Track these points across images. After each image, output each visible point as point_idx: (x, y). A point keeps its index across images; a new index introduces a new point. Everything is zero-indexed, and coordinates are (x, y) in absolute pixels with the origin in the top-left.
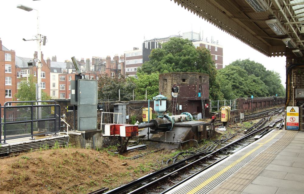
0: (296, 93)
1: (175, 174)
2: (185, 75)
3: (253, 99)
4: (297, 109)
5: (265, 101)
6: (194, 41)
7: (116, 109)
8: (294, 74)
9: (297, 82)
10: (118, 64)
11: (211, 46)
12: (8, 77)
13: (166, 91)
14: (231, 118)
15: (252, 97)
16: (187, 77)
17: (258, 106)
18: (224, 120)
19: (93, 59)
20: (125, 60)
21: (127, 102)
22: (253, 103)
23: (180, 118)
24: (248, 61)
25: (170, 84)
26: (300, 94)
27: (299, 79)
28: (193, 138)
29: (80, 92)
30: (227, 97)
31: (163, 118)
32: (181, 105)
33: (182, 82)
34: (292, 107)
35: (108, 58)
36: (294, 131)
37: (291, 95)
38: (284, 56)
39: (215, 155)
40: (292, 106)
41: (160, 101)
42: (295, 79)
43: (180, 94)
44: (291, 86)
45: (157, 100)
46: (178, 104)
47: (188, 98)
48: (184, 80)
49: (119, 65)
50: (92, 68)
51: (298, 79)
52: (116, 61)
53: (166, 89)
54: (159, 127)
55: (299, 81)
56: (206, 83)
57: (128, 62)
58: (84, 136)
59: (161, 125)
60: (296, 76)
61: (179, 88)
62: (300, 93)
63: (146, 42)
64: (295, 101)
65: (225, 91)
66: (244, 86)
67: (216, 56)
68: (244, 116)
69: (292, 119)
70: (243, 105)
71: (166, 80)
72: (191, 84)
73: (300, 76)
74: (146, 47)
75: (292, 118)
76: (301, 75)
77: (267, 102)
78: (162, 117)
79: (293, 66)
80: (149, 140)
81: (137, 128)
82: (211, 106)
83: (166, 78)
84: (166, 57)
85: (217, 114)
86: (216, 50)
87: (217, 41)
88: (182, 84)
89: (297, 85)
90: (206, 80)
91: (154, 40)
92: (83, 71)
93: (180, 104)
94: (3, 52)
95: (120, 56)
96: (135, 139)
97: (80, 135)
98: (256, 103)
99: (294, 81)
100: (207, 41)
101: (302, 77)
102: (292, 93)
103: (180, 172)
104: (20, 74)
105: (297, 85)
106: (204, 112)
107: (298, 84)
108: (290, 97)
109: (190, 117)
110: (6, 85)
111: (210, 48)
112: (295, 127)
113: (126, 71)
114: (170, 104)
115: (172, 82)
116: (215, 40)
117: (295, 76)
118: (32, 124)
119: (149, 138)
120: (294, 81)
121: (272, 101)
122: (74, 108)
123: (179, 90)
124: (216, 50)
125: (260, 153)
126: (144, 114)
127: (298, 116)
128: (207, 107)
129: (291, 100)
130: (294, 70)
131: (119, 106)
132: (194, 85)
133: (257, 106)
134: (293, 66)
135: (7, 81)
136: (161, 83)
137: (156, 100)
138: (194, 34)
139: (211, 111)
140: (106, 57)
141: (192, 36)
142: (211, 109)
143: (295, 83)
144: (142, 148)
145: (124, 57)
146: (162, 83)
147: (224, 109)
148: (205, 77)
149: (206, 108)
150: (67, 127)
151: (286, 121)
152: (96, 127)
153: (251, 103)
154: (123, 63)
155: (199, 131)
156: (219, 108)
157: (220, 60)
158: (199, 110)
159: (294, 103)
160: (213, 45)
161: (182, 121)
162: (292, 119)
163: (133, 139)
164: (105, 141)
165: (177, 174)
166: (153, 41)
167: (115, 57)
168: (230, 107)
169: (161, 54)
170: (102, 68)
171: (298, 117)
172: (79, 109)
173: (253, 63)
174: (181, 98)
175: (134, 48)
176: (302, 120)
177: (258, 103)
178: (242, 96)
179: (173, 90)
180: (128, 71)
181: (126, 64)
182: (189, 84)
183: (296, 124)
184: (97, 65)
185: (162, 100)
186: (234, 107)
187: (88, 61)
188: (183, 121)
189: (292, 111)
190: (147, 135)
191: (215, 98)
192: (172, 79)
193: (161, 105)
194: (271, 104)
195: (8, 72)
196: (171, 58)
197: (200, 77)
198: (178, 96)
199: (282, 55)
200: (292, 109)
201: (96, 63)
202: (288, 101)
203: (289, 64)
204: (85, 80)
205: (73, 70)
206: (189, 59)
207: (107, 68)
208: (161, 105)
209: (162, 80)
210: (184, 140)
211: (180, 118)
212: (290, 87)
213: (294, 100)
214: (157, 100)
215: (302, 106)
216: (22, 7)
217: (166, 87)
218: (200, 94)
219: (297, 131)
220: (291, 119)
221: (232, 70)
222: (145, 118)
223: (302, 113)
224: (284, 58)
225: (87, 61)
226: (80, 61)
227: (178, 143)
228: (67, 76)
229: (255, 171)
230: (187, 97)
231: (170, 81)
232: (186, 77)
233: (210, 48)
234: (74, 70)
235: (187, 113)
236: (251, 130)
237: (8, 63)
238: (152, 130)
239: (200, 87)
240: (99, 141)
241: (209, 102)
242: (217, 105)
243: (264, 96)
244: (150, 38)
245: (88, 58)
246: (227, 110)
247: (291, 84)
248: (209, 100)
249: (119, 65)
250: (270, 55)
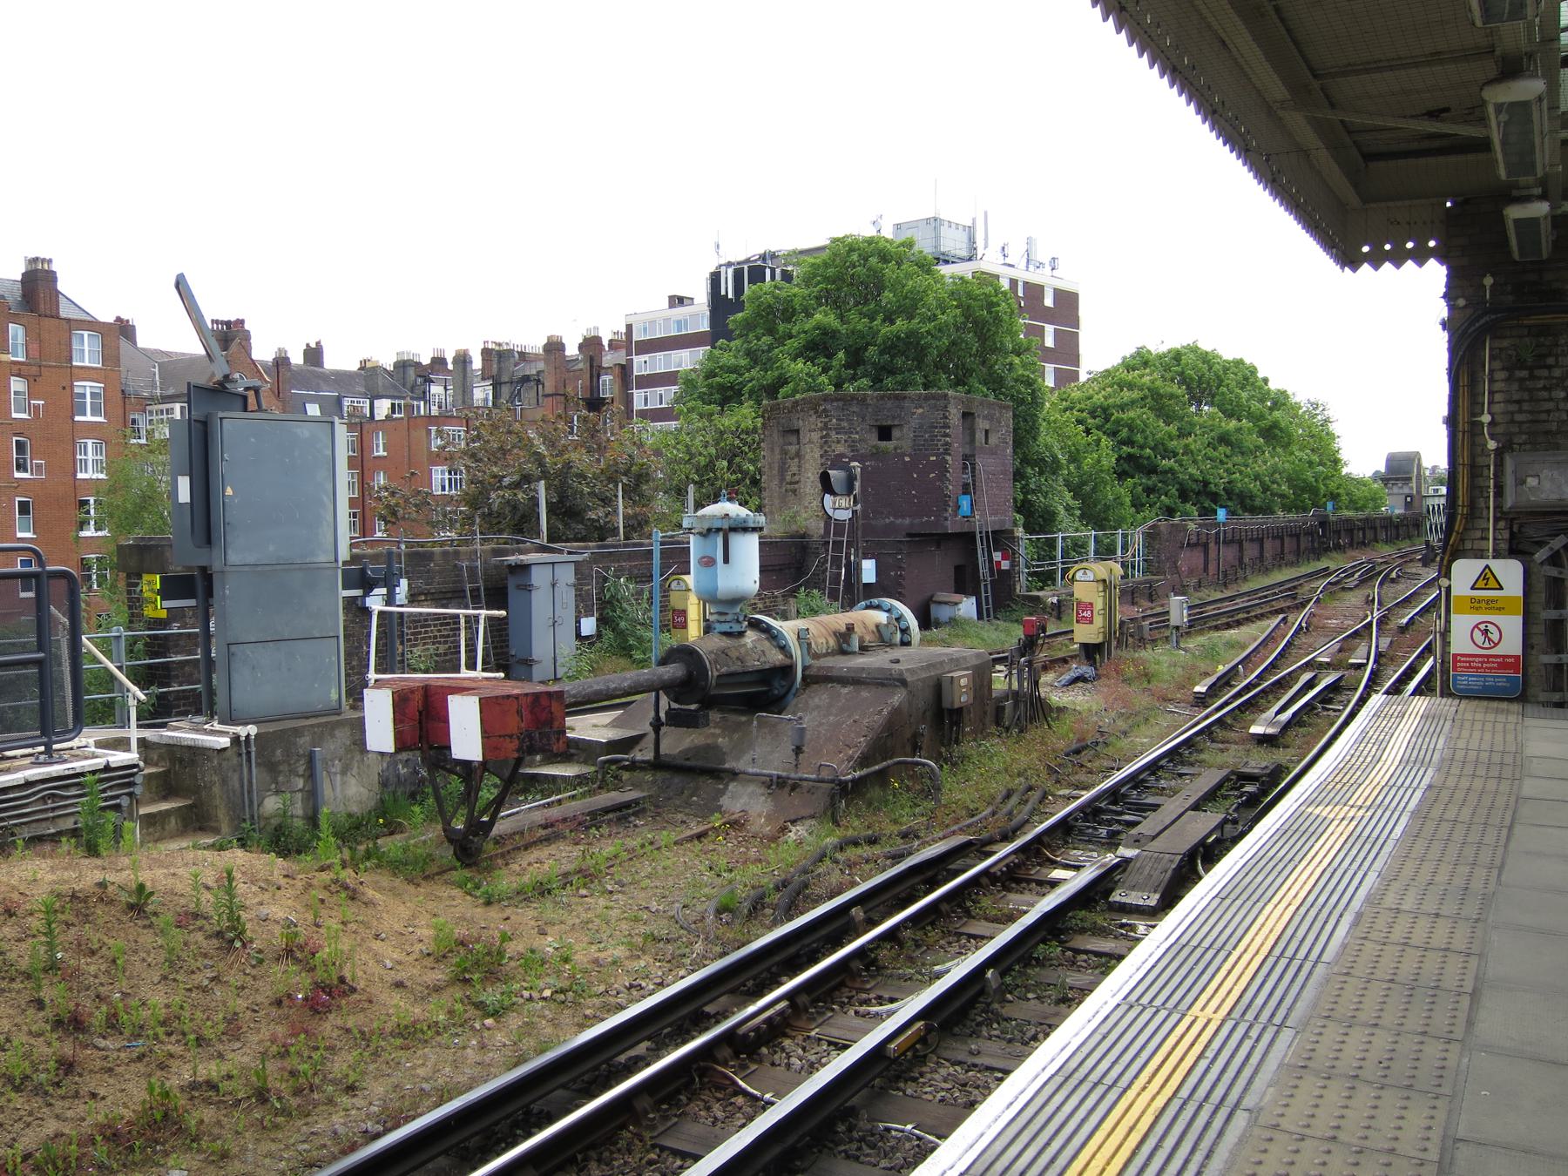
0: (1509, 480)
1: (769, 1019)
2: (889, 404)
3: (1224, 525)
4: (1510, 573)
5: (1279, 535)
6: (947, 262)
7: (518, 587)
8: (1497, 364)
9: (1512, 413)
11: (1026, 284)
12: (90, 442)
13: (794, 491)
14: (1122, 623)
15: (1221, 514)
16: (899, 416)
17: (1246, 560)
18: (1087, 633)
19: (486, 353)
20: (629, 353)
21: (586, 548)
22: (1224, 542)
24: (1194, 349)
25: (817, 455)
26: (1531, 482)
27: (1526, 396)
28: (916, 749)
29: (229, 491)
30: (1094, 515)
31: (741, 634)
33: (873, 439)
34: (1483, 562)
35: (554, 347)
36: (1495, 704)
37: (1476, 490)
38: (1432, 264)
39: (1038, 853)
40: (1480, 554)
42: (1498, 397)
43: (865, 503)
44: (1478, 440)
45: (708, 533)
46: (856, 556)
47: (907, 521)
48: (885, 433)
49: (606, 378)
50: (481, 393)
51: (1516, 397)
52: (592, 359)
53: (797, 478)
54: (718, 685)
55: (1526, 406)
57: (642, 365)
58: (249, 753)
59: (728, 678)
60: (1507, 380)
62: (1529, 480)
63: (723, 270)
64: (1502, 524)
67: (1049, 330)
68: (1190, 608)
69: (1485, 632)
71: (797, 431)
73: (1532, 377)
74: (723, 293)
75: (1482, 627)
76: (1537, 372)
77: (1287, 540)
79: (1487, 318)
80: (659, 764)
81: (555, 707)
84: (809, 325)
85: (1055, 600)
86: (1049, 301)
87: (1054, 259)
88: (876, 454)
89: (1515, 429)
90: (998, 431)
91: (763, 257)
92: (440, 407)
94: (66, 326)
95: (610, 337)
97: (224, 749)
98: (1240, 543)
99: (1497, 408)
100: (1008, 261)
101: (1541, 384)
102: (1481, 482)
103: (803, 999)
104: (143, 426)
105: (1515, 429)
106: (986, 592)
107: (1521, 423)
108: (1472, 505)
110: (80, 476)
111: (1020, 294)
112: (1500, 678)
113: (638, 404)
114: (817, 555)
116: (1043, 255)
117: (1501, 375)
118: (41, 674)
119: (663, 751)
120: (1497, 408)
121: (1310, 533)
122: (200, 586)
123: (857, 484)
124: (1049, 301)
125: (1359, 916)
126: (679, 607)
127: (1517, 614)
128: (1005, 565)
129: (1481, 524)
130: (1497, 344)
131: (534, 568)
132: (937, 455)
133: (1241, 559)
134: (1487, 318)
135: (83, 457)
136: (772, 450)
137: (700, 534)
138: (944, 230)
139: (1021, 586)
140: (545, 341)
141: (937, 238)
143: (1499, 418)
144: (622, 814)
145: (627, 343)
146: (777, 451)
147: (1090, 576)
148: (990, 418)
149: (1001, 572)
150: (132, 703)
151: (1446, 644)
152: (334, 696)
153: (1217, 543)
154: (623, 367)
156: (1065, 571)
157: (1068, 350)
158: (965, 582)
159: (1495, 539)
160: (1034, 277)
162: (1485, 632)
163: (573, 755)
164: (398, 776)
165: (781, 1013)
166: (759, 263)
167: (585, 339)
168: (1118, 569)
169: (789, 314)
170: (529, 394)
171: (1517, 621)
172: (228, 591)
173: (1207, 358)
174: (873, 522)
175: (672, 298)
176: (1539, 640)
177: (1246, 545)
178: (1170, 512)
179: (827, 486)
180: (646, 404)
181: (635, 373)
182: (910, 450)
183: (1504, 663)
184: (505, 378)
185: (734, 529)
186: (1133, 567)
187: (463, 359)
188: (864, 649)
189: (1481, 584)
191: (1039, 520)
192: (825, 427)
193: (726, 560)
194: (1306, 549)
195: (89, 418)
196: (827, 333)
197: (967, 415)
199: (1420, 257)
200: (1487, 578)
201: (500, 369)
202: (1458, 525)
203: (1465, 307)
204: (263, 416)
205: (393, 405)
206: (911, 334)
207: (549, 390)
208: (726, 560)
209: (775, 435)
210: (864, 761)
212: (1473, 444)
213: (1496, 520)
214: (708, 533)
215: (1541, 555)
216: (181, 285)
217: (794, 469)
219: (1516, 707)
220: (1477, 634)
221: (1121, 385)
223: (1541, 596)
224: (1435, 274)
225: (455, 361)
226: (426, 361)
227: (822, 781)
228: (364, 432)
229: (1286, 955)
230: (903, 517)
231: (815, 436)
232: (894, 418)
233: (1020, 294)
234: (399, 405)
235: (888, 601)
236: (1228, 684)
237: (87, 373)
238: (675, 706)
239: (965, 467)
240: (353, 781)
241: (1013, 539)
242: (1054, 558)
243: (1267, 510)
244: (743, 249)
245: (463, 347)
246: (1104, 581)
247: (1475, 427)
248: (1012, 532)
249: (603, 378)
250: (1348, 258)
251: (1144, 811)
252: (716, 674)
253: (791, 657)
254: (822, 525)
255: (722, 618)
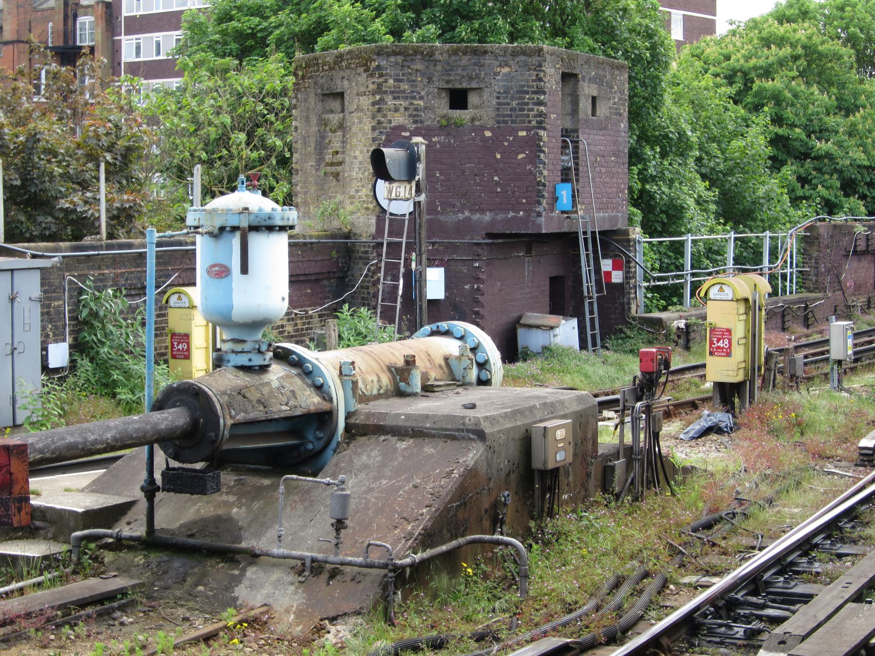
2: (465, 60)
10: (75, 17)
13: (336, 175)
14: (769, 356)
16: (478, 77)
23: (401, 363)
25: (368, 127)
32: (441, 271)
33: (442, 106)
41: (236, 241)
43: (431, 191)
47: (487, 217)
48: (458, 99)
53: (339, 157)
54: (233, 437)
56: (607, 118)
61: (423, 148)
65: (730, 172)
66: (840, 144)
70: (840, 265)
71: (341, 95)
72: (503, 127)
78: (257, 361)
82: (639, 272)
83: (342, 85)
93: (431, 263)
96: (52, 530)
106: (591, 312)
109: (481, 358)
113: (127, 56)
115: (379, 106)
123: (421, 167)
128: (617, 277)
132: (528, 130)
137: (210, 234)
142: (641, 293)
146: (314, 120)
147: (728, 293)
148: (598, 80)
155: (537, 464)
156: (695, 286)
161: (417, 387)
163: (38, 529)
168: (764, 285)
178: (831, 207)
180: (138, 53)
185: (254, 229)
188: (428, 389)
190: (141, 510)
192: (379, 90)
193: (244, 270)
198: (417, 204)
208: (244, 270)
209: (312, 100)
210: (427, 539)
211: (401, 363)
217: (336, 145)
218: (564, 193)
222: (187, 356)
230: (482, 211)
231: (366, 102)
232: (471, 79)
235: (461, 326)
239: (565, 146)
242: (680, 268)
246: (746, 300)
248: (626, 233)
249: (81, 19)
251: (793, 603)
252: (230, 422)
253: (331, 400)
254: (373, 221)
255: (239, 347)
